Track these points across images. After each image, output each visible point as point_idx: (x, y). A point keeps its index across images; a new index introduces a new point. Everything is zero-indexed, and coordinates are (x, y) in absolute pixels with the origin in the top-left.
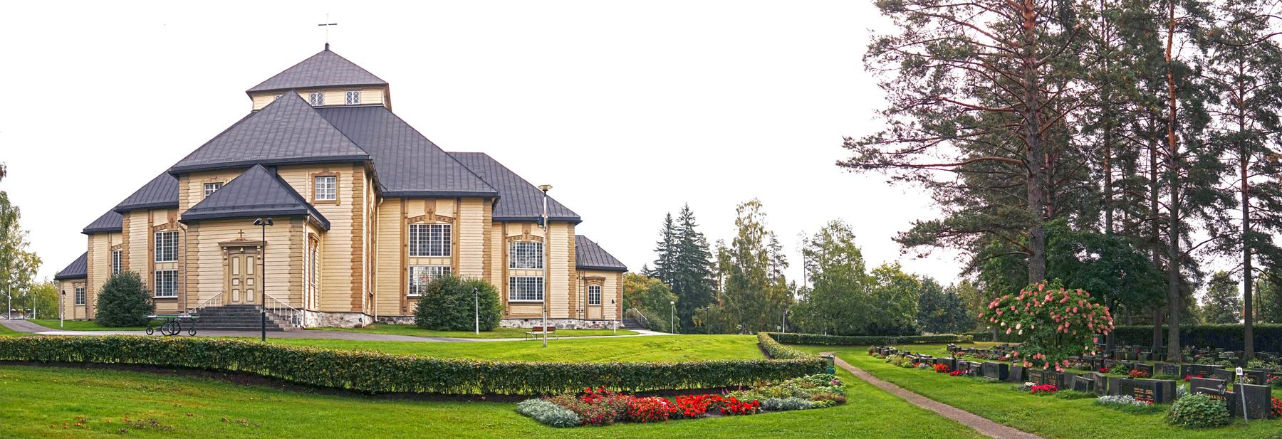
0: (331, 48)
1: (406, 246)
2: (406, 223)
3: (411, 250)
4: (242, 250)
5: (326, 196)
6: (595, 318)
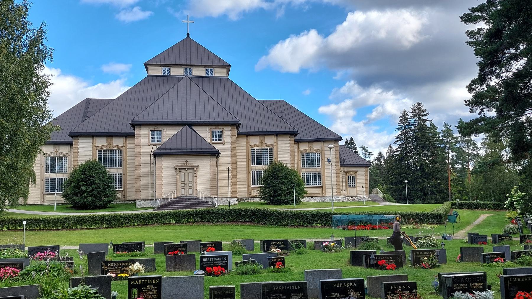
1: (249, 160)
2: (249, 148)
3: (252, 162)
4: (186, 170)
5: (217, 140)
6: (353, 195)
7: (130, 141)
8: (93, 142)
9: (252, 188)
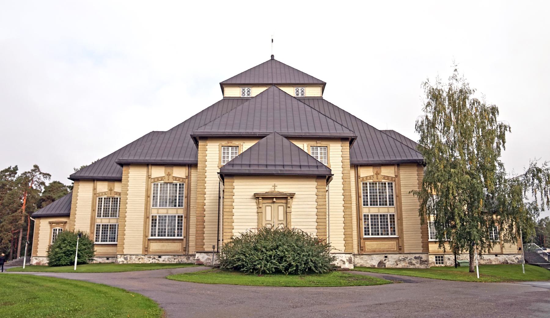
0: (275, 58)
7: (193, 171)
8: (148, 172)
9: (149, 240)
